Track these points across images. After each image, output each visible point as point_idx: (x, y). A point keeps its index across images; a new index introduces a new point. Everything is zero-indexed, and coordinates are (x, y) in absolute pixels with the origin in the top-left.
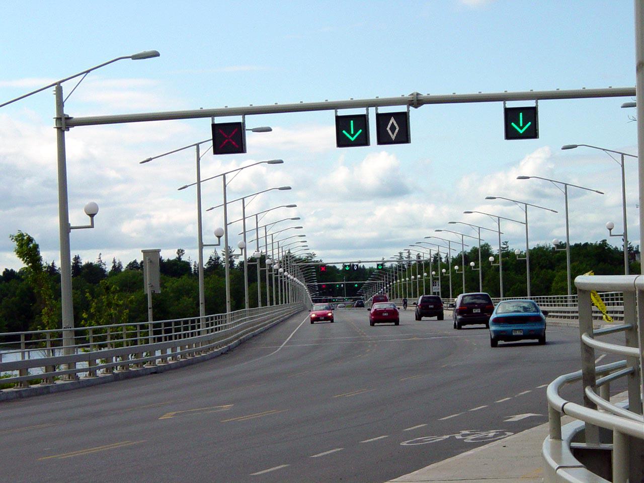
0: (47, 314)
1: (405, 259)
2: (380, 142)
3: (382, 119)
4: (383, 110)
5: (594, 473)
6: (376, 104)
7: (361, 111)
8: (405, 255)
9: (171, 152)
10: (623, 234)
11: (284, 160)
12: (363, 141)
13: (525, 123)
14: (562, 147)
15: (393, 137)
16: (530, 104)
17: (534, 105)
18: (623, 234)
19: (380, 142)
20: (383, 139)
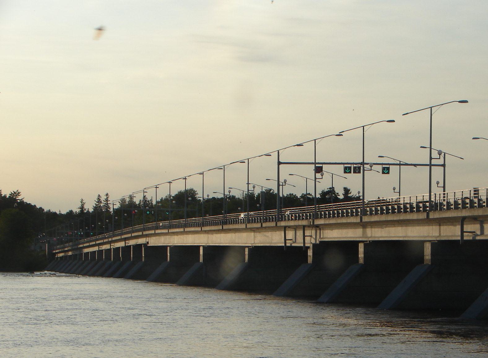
0: (43, 236)
1: (103, 202)
2: (354, 173)
3: (355, 168)
4: (355, 166)
5: (332, 241)
6: (353, 164)
7: (350, 165)
8: (103, 198)
9: (248, 169)
10: (365, 171)
11: (245, 162)
12: (350, 172)
13: (387, 171)
14: (378, 156)
15: (357, 172)
16: (388, 166)
17: (389, 167)
18: (365, 171)
19: (354, 173)
20: (355, 172)
